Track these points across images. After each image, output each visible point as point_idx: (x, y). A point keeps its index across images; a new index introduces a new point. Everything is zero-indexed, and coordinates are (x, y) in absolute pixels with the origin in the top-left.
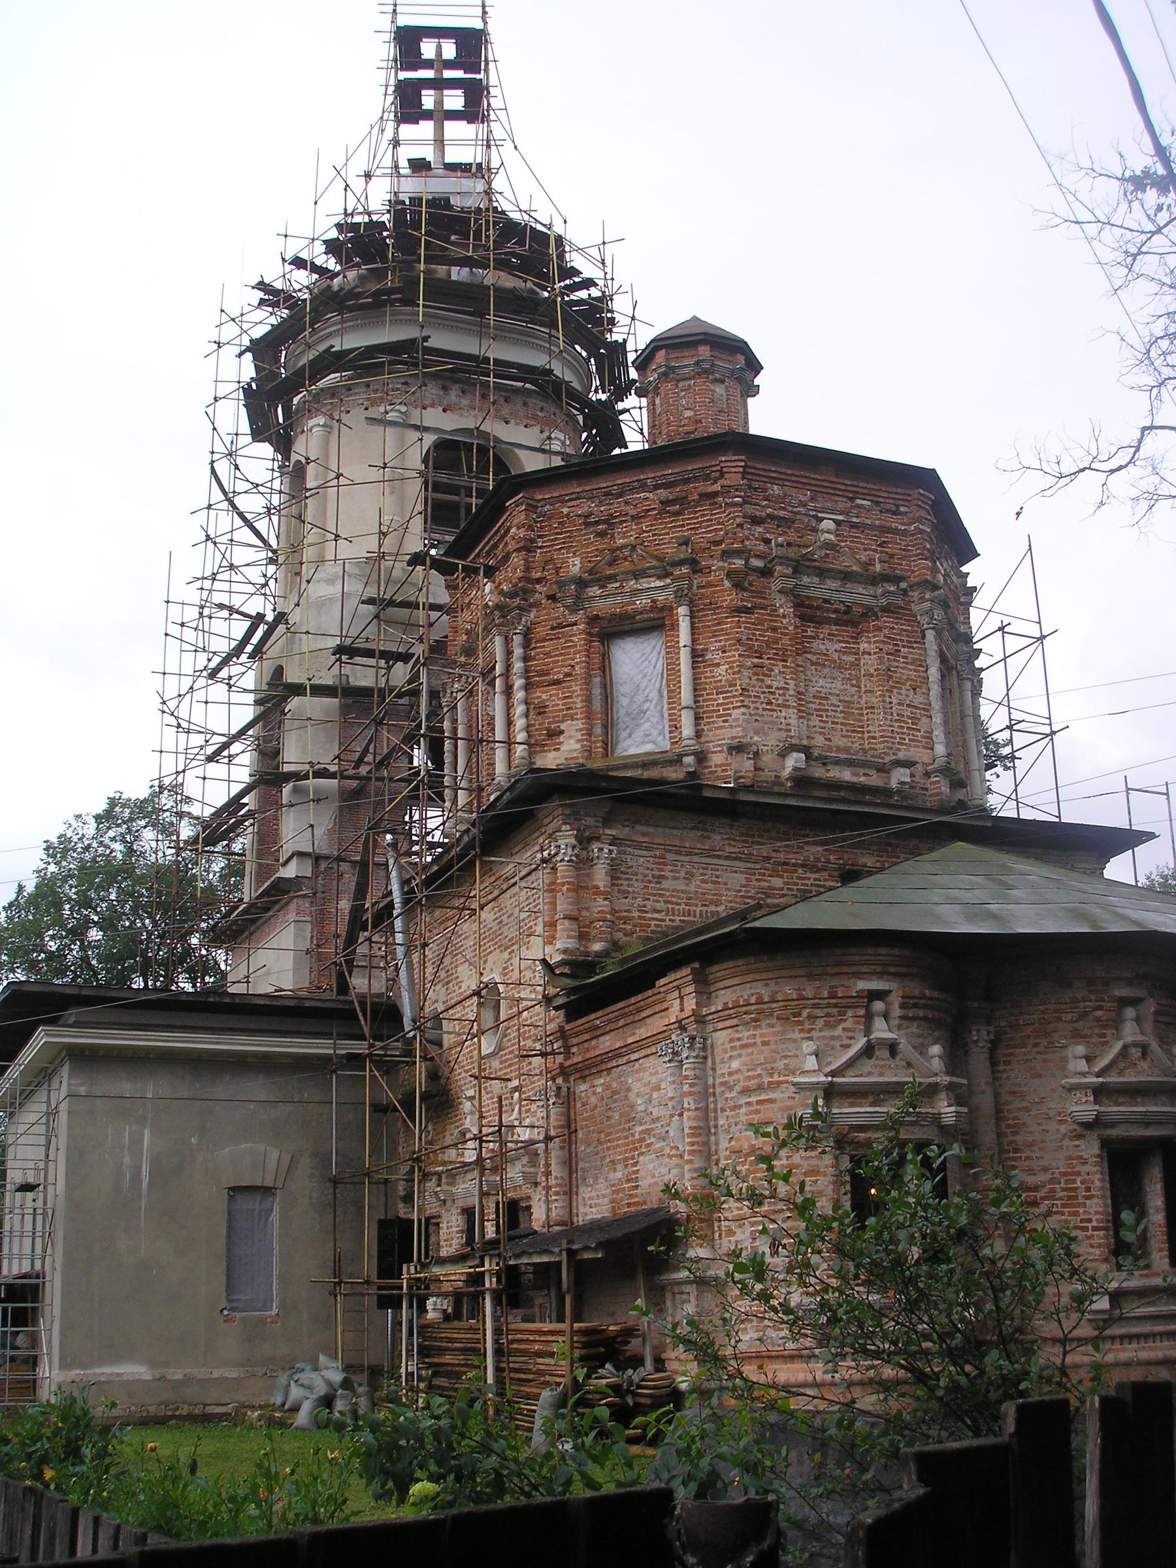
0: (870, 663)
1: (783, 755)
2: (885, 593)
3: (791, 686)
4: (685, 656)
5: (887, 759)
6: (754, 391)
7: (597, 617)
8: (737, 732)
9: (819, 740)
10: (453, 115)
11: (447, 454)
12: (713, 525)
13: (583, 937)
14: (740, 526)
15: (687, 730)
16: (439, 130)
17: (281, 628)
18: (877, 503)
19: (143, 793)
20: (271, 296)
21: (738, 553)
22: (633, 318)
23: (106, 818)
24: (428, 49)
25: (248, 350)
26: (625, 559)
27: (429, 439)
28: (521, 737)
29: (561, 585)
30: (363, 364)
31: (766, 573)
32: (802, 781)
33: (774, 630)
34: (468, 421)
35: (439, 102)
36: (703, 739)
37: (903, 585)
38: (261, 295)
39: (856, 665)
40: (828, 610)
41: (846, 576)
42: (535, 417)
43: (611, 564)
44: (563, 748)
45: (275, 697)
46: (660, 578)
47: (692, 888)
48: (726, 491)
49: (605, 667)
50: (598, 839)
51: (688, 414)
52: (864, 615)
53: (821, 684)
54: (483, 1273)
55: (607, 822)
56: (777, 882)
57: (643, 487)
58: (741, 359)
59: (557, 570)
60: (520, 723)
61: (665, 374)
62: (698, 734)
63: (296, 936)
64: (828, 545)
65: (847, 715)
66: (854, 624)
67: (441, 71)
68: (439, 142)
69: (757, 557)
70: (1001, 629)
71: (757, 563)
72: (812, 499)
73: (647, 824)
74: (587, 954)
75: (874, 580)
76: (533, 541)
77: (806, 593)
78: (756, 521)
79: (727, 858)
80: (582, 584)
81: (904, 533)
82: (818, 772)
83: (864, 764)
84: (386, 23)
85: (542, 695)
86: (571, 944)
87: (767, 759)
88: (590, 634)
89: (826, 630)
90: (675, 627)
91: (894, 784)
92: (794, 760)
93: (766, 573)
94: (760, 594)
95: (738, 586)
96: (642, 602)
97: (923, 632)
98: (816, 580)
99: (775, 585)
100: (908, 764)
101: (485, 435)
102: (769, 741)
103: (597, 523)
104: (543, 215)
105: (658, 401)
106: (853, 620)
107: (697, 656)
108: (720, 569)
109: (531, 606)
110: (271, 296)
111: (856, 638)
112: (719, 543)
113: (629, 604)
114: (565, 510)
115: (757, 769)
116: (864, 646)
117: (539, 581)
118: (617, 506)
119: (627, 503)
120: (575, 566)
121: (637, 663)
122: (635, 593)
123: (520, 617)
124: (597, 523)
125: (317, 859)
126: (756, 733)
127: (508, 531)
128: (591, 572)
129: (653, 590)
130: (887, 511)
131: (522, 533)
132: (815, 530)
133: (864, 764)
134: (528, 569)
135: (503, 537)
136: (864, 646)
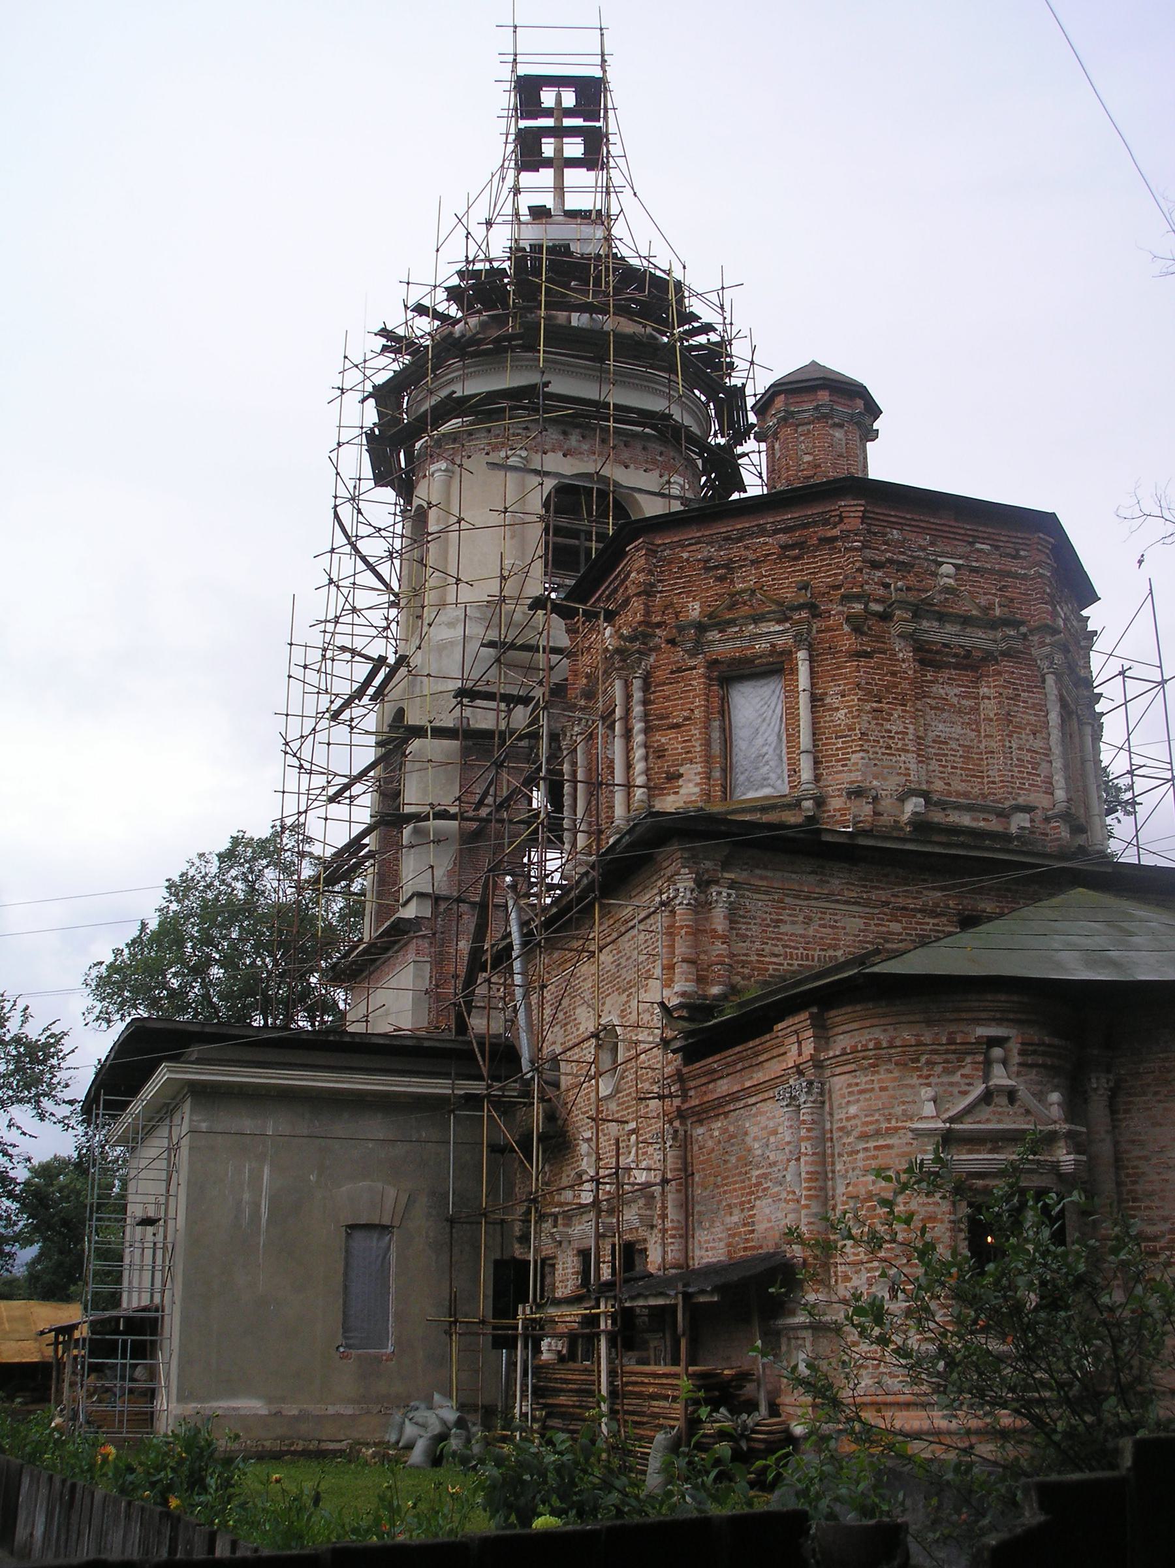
0: (989, 708)
1: (902, 799)
2: (1005, 638)
3: (911, 731)
4: (804, 700)
5: (1007, 804)
6: (873, 435)
7: (716, 661)
8: (856, 776)
9: (939, 785)
10: (573, 163)
11: (567, 498)
12: (829, 570)
13: (701, 980)
14: (860, 570)
15: (806, 774)
16: (559, 177)
17: (403, 671)
18: (997, 548)
19: (265, 833)
20: (394, 342)
21: (857, 598)
22: (752, 363)
23: (228, 857)
24: (548, 98)
25: (370, 395)
26: (745, 603)
27: (550, 484)
28: (640, 780)
29: (681, 629)
30: (484, 410)
31: (885, 617)
32: (921, 826)
33: (894, 674)
34: (588, 466)
35: (559, 150)
36: (821, 784)
37: (1023, 629)
38: (383, 341)
39: (975, 710)
40: (947, 655)
41: (966, 621)
42: (654, 462)
43: (730, 608)
44: (682, 791)
45: (396, 739)
46: (779, 622)
47: (811, 932)
48: (845, 536)
49: (724, 711)
50: (717, 882)
51: (807, 458)
52: (984, 659)
53: (940, 729)
54: (598, 1315)
55: (726, 865)
56: (895, 927)
57: (763, 532)
58: (860, 403)
59: (677, 615)
60: (639, 766)
61: (784, 419)
62: (817, 778)
63: (416, 977)
64: (947, 590)
65: (967, 759)
66: (974, 668)
67: (559, 117)
68: (559, 189)
69: (876, 601)
70: (1122, 673)
71: (876, 607)
72: (932, 544)
73: (765, 868)
74: (705, 997)
75: (994, 624)
76: (652, 585)
77: (925, 637)
78: (875, 565)
79: (846, 903)
80: (701, 628)
81: (1024, 577)
82: (937, 817)
83: (984, 809)
84: (506, 73)
85: (661, 738)
86: (689, 987)
87: (886, 804)
88: (709, 678)
89: (945, 674)
90: (794, 671)
91: (1013, 830)
92: (913, 805)
93: (885, 617)
94: (879, 638)
95: (857, 630)
96: (761, 646)
97: (1043, 676)
98: (936, 624)
99: (895, 629)
100: (1028, 809)
101: (605, 480)
102: (888, 786)
103: (716, 568)
104: (662, 261)
105: (777, 446)
106: (972, 664)
107: (816, 700)
108: (840, 613)
109: (651, 650)
110: (394, 342)
111: (976, 682)
112: (839, 587)
113: (748, 648)
114: (685, 555)
115: (877, 814)
116: (984, 690)
117: (659, 625)
118: (737, 550)
119: (746, 548)
120: (695, 610)
121: (756, 709)
122: (755, 637)
123: (640, 660)
124: (716, 568)
125: (437, 899)
126: (876, 778)
127: (628, 575)
128: (710, 616)
129: (773, 634)
130: (1007, 555)
131: (642, 578)
132: (934, 574)
133: (984, 809)
134: (647, 613)
135: (623, 581)
136: (984, 690)
